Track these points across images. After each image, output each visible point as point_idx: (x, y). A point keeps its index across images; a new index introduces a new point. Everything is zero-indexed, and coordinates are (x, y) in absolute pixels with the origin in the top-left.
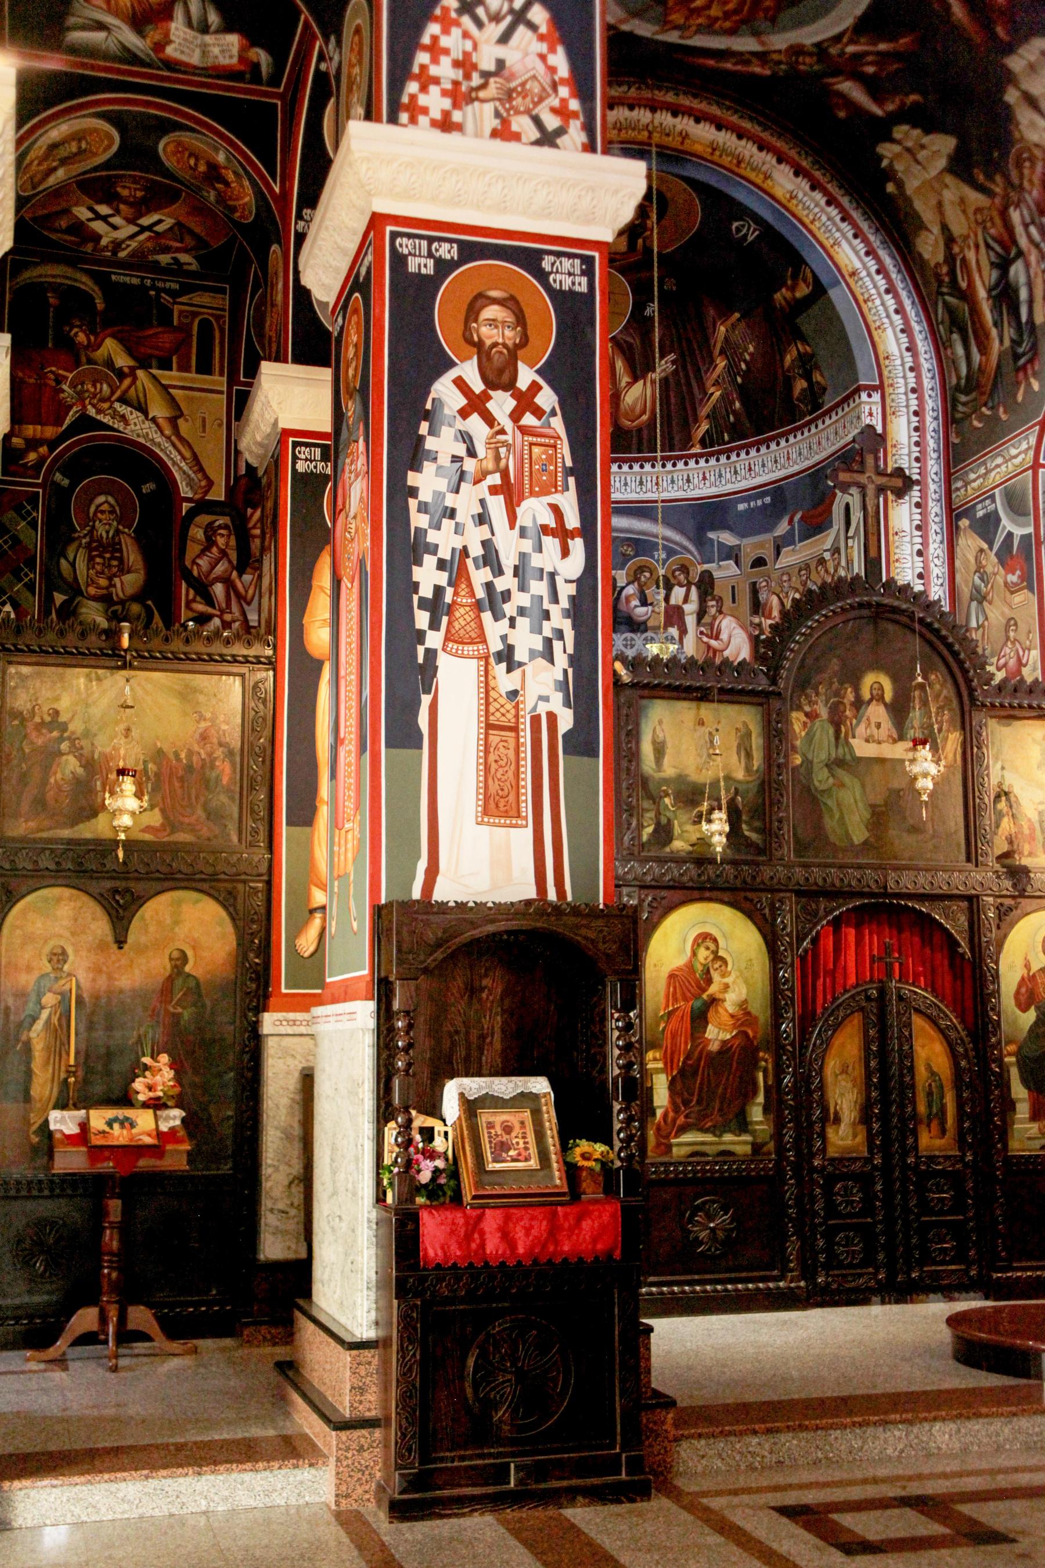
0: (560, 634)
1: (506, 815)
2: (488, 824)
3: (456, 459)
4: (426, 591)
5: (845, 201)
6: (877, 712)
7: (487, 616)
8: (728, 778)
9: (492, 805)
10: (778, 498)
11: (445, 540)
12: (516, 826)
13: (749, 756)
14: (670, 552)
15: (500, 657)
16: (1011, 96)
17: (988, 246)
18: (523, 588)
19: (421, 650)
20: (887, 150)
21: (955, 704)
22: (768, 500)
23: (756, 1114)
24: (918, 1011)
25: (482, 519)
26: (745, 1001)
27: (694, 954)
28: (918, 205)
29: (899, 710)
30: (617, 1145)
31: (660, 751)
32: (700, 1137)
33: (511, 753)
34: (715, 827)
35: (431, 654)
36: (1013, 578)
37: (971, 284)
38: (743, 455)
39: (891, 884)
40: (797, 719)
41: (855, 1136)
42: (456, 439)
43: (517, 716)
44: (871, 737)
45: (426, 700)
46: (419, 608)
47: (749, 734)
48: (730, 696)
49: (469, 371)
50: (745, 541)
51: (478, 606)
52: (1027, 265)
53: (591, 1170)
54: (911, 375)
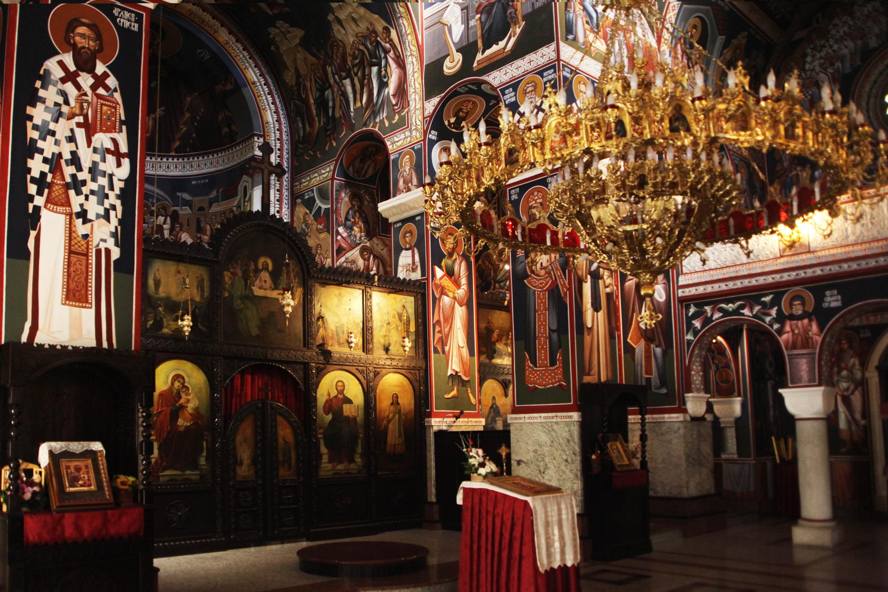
0: (114, 207)
1: (79, 301)
2: (69, 305)
3: (56, 104)
4: (35, 173)
5: (252, 50)
6: (265, 276)
7: (72, 193)
8: (192, 300)
9: (71, 295)
10: (212, 180)
11: (48, 147)
12: (85, 307)
13: (202, 290)
14: (158, 200)
15: (78, 215)
16: (331, 17)
17: (316, 81)
18: (94, 180)
19: (31, 206)
20: (273, 31)
21: (301, 276)
22: (207, 181)
23: (202, 461)
24: (280, 414)
25: (72, 139)
26: (198, 408)
27: (172, 384)
28: (285, 58)
29: (275, 276)
30: (141, 477)
31: (157, 283)
32: (174, 472)
33: (84, 268)
34: (185, 323)
35: (37, 209)
36: (320, 227)
37: (307, 96)
38: (196, 159)
39: (269, 355)
40: (227, 276)
41: (249, 471)
42: (58, 93)
43: (87, 248)
44: (262, 287)
45: (33, 234)
46: (31, 182)
47: (203, 280)
48: (193, 261)
49: (68, 59)
50: (195, 199)
51: (67, 186)
52: (333, 92)
53: (126, 490)
54: (278, 132)
